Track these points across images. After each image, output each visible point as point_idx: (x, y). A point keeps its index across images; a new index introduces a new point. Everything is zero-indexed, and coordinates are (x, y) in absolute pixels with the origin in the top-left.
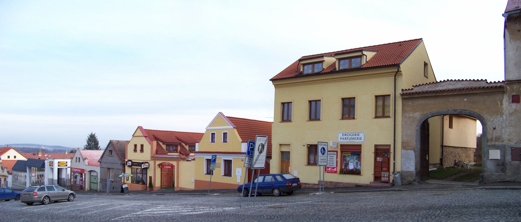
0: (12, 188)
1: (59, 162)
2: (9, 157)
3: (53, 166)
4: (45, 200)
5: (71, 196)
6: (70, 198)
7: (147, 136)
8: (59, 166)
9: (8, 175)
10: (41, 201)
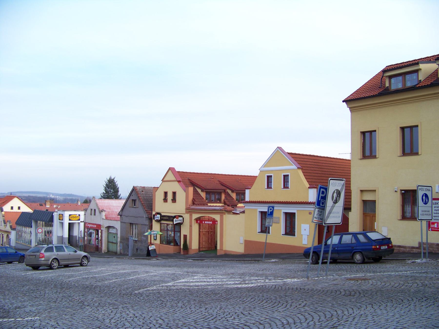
0: (15, 247)
1: (70, 215)
2: (12, 208)
3: (62, 220)
4: (53, 264)
8: (70, 220)
9: (11, 231)
10: (48, 264)
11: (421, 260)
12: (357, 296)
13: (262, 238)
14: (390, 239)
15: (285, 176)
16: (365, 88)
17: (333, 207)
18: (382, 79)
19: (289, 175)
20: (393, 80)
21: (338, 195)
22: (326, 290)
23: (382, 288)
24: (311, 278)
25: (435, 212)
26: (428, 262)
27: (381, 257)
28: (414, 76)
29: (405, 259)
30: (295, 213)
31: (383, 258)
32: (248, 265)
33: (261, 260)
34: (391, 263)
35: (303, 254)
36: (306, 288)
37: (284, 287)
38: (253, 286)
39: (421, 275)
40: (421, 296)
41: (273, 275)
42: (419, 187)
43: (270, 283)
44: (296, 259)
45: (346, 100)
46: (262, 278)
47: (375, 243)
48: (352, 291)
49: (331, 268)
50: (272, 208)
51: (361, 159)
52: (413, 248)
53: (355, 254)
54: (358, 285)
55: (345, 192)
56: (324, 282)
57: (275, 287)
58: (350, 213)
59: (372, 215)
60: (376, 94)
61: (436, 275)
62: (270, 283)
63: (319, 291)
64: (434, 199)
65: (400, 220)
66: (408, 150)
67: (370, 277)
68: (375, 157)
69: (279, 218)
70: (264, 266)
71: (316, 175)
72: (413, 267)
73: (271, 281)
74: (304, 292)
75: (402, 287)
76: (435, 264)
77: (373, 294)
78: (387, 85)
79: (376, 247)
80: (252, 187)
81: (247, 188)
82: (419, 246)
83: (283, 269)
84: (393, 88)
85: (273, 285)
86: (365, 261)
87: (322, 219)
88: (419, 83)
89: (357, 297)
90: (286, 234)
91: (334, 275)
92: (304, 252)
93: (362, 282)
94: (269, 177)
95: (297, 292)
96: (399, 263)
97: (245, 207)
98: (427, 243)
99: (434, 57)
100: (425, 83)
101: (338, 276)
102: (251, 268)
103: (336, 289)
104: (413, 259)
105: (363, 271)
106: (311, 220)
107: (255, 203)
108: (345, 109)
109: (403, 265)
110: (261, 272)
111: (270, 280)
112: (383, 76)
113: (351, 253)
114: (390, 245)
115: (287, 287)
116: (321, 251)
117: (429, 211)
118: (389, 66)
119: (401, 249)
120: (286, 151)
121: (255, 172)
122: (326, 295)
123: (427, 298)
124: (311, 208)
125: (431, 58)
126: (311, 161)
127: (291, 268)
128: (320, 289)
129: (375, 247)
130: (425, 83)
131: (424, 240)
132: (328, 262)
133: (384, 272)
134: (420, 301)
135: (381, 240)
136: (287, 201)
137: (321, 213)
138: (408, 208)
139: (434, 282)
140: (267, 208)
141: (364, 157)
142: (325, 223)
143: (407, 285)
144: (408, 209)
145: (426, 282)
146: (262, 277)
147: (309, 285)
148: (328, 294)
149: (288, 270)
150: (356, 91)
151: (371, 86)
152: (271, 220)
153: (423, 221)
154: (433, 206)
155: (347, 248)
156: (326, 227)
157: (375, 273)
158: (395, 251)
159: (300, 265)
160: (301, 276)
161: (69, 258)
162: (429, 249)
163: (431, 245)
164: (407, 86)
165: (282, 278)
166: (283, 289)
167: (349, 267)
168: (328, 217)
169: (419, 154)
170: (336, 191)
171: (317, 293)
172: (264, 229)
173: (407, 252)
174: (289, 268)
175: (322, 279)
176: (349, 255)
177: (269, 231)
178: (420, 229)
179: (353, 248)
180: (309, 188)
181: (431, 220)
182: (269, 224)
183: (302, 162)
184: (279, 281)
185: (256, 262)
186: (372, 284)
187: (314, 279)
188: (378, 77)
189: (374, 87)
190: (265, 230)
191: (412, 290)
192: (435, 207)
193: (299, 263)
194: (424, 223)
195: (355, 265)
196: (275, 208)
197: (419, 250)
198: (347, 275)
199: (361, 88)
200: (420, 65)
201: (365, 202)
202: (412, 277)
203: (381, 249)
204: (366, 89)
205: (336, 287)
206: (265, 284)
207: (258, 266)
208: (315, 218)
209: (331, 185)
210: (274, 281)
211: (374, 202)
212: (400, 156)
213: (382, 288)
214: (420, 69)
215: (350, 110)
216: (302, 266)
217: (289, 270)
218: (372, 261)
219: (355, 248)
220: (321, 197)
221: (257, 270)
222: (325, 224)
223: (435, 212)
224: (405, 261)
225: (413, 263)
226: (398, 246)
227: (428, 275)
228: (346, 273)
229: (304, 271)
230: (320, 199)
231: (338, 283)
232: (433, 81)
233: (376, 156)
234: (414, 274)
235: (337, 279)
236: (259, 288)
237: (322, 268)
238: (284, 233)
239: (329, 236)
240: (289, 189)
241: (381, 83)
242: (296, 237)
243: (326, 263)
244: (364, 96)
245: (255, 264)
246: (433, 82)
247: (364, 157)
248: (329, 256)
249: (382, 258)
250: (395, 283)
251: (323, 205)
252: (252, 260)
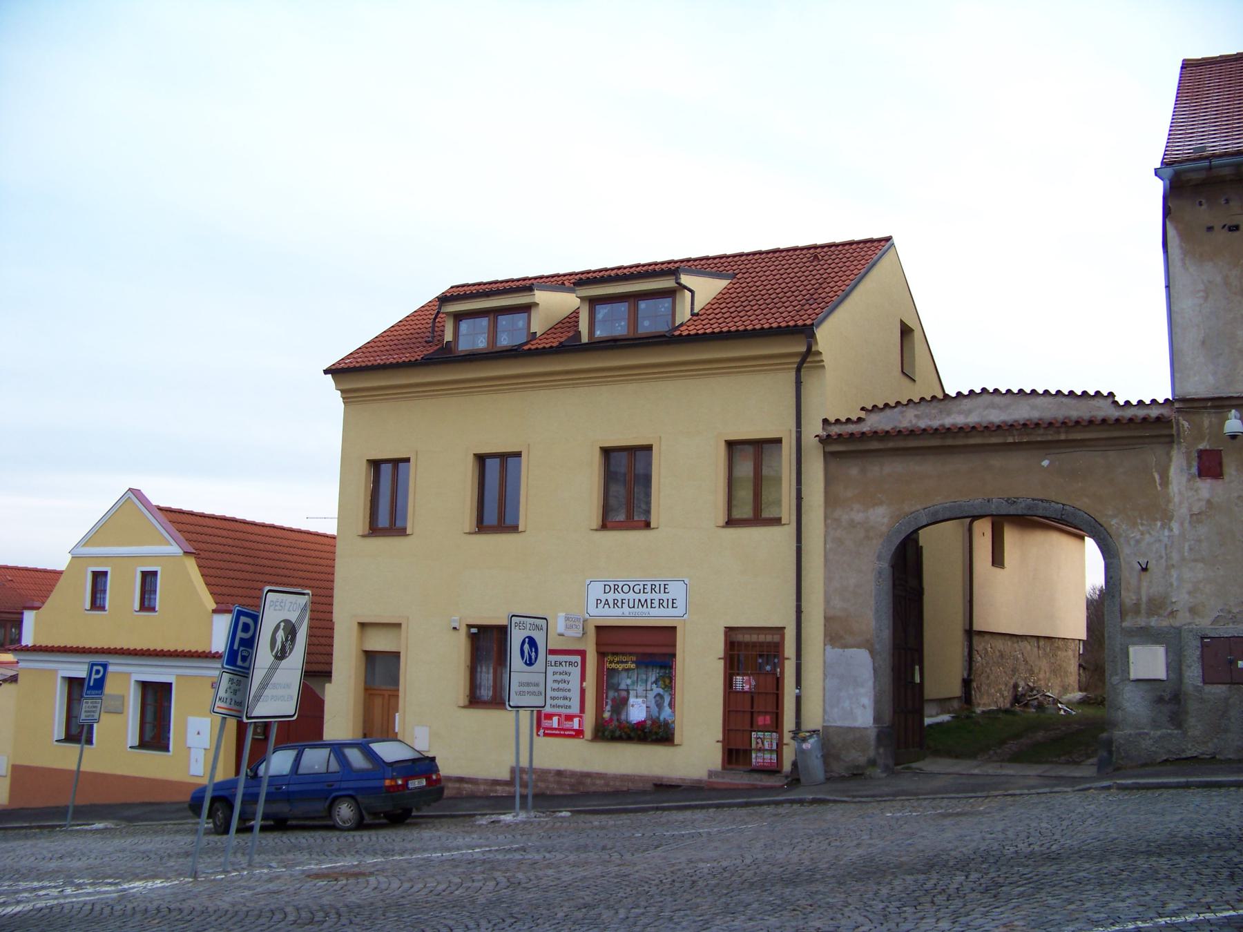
11: (514, 816)
12: (331, 924)
13: (67, 758)
14: (433, 759)
15: (96, 575)
16: (388, 339)
17: (273, 669)
18: (435, 319)
19: (109, 574)
20: (464, 326)
21: (287, 637)
22: (245, 909)
23: (403, 897)
24: (204, 875)
25: (556, 686)
26: (532, 820)
27: (410, 811)
28: (520, 320)
29: (475, 815)
30: (170, 684)
31: (413, 814)
32: (15, 844)
33: (59, 826)
34: (434, 826)
35: (186, 806)
36: (185, 905)
37: (119, 908)
38: (20, 912)
39: (508, 857)
40: (502, 914)
41: (90, 871)
42: (513, 618)
43: (76, 896)
44: (172, 819)
45: (333, 367)
46: (53, 884)
47: (393, 771)
48: (317, 911)
49: (266, 845)
50: (101, 669)
51: (363, 536)
52: (496, 782)
53: (338, 801)
54: (336, 891)
55: (311, 627)
56: (240, 887)
57: (92, 910)
58: (327, 685)
59: (390, 693)
60: (416, 360)
61: (548, 855)
62: (76, 896)
63: (224, 913)
64: (553, 652)
65: (464, 707)
66: (491, 517)
67: (373, 866)
68: (402, 532)
69: (122, 699)
70: (68, 842)
71: (238, 574)
72: (490, 835)
73: (80, 891)
74: (177, 920)
75: (457, 892)
76: (548, 826)
77: (374, 916)
78: (448, 337)
79: (396, 782)
80: (43, 603)
81: (28, 605)
82: (511, 778)
83: (123, 850)
84: (464, 346)
85: (85, 903)
86: (365, 822)
87: (240, 704)
88: (531, 341)
89: (331, 927)
90: (143, 744)
91: (274, 864)
92: (193, 799)
93: (349, 882)
94: (98, 578)
95: (157, 921)
96: (456, 825)
97: (17, 662)
98: (532, 770)
99: (572, 277)
100: (546, 341)
101: (285, 867)
102: (23, 852)
103: (273, 907)
104: (493, 814)
105: (357, 852)
106: (208, 707)
107: (53, 651)
108: (330, 395)
109: (467, 832)
110: (53, 865)
111: (79, 886)
112: (438, 313)
113: (327, 798)
114: (434, 777)
115: (130, 906)
116: (235, 795)
117: (537, 685)
118: (458, 287)
119: (466, 786)
120: (155, 503)
121: (57, 560)
122: (242, 926)
123: (516, 918)
124: (213, 671)
125: (566, 277)
126: (225, 533)
127: (150, 846)
128: (226, 906)
129: (393, 783)
130: (546, 341)
131: (524, 763)
132: (257, 829)
133: (414, 851)
134: (496, 928)
135: (410, 763)
136: (149, 650)
137: (237, 687)
138: (484, 676)
139: (540, 873)
140: (86, 667)
141: (374, 530)
142: (249, 715)
143: (470, 884)
144: (486, 677)
145: (520, 875)
146: (55, 880)
147: (196, 896)
148: (247, 921)
149: (140, 855)
150: (365, 346)
151: (404, 337)
152: (96, 702)
153: (522, 711)
154: (550, 670)
155: (314, 787)
156: (252, 726)
157: (388, 855)
158: (446, 793)
159: (178, 837)
160: (177, 870)
162: (536, 786)
163: (543, 774)
164: (498, 345)
165: (117, 881)
166: (117, 914)
167: (319, 841)
168: (258, 698)
169: (520, 530)
170: (282, 624)
171: (216, 920)
172: (74, 731)
173: (479, 794)
174: (142, 848)
175: (235, 878)
176: (320, 806)
177: (92, 737)
178: (514, 733)
179: (332, 786)
180: (215, 611)
181: (543, 707)
182: (88, 716)
183: (199, 538)
184: (106, 889)
185: (46, 831)
186: (376, 888)
187: (214, 880)
188: (419, 318)
189: (414, 340)
190: (78, 733)
191: (482, 900)
192: (554, 673)
193: (177, 832)
194: (525, 716)
195: (337, 833)
196: (111, 668)
197: (512, 789)
198: (310, 864)
199: (377, 339)
200: (536, 292)
201: (370, 657)
202: (484, 862)
203: (408, 788)
204: (391, 343)
205: (274, 901)
206: (62, 901)
207: (47, 844)
208: (220, 699)
209: (270, 606)
210: (90, 889)
211: (396, 655)
212: (470, 533)
213: (403, 897)
214: (536, 305)
215: (344, 398)
216: (184, 841)
217: (144, 852)
218: (384, 821)
219: (336, 785)
220: (241, 639)
221: (44, 859)
222: (248, 718)
223: (556, 686)
224: (473, 819)
225: (492, 825)
226: (457, 777)
227: (526, 857)
228: (307, 856)
229: (187, 854)
230: (236, 647)
231: (281, 889)
232: (566, 338)
233: (405, 529)
234: (491, 856)
235: (278, 877)
236: (40, 914)
237: (242, 843)
238: (136, 743)
239: (260, 754)
240: (157, 614)
241: (434, 331)
242: (171, 753)
243: (250, 829)
244: (349, 365)
245: (40, 838)
246: (566, 340)
247: (374, 530)
248: (260, 808)
249: (411, 813)
250: (438, 883)
251: (246, 665)
252: (31, 828)
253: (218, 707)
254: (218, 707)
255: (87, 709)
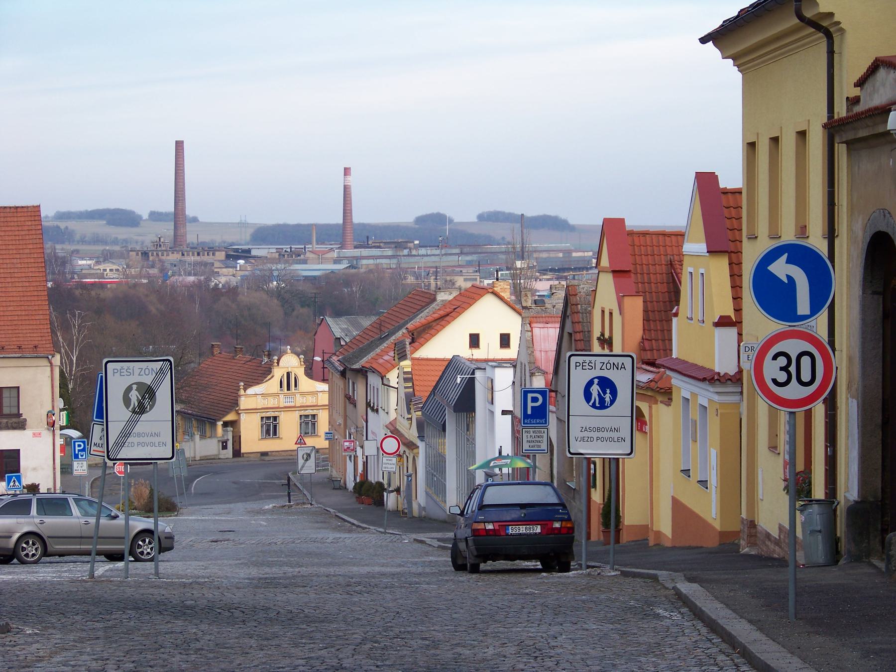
2: (474, 341)
4: (24, 549)
5: (144, 541)
6: (140, 546)
7: (631, 268)
10: (9, 549)
17: (304, 464)
152: (540, 432)
161: (83, 535)
253: (94, 451)
254: (94, 451)
255: (529, 439)
